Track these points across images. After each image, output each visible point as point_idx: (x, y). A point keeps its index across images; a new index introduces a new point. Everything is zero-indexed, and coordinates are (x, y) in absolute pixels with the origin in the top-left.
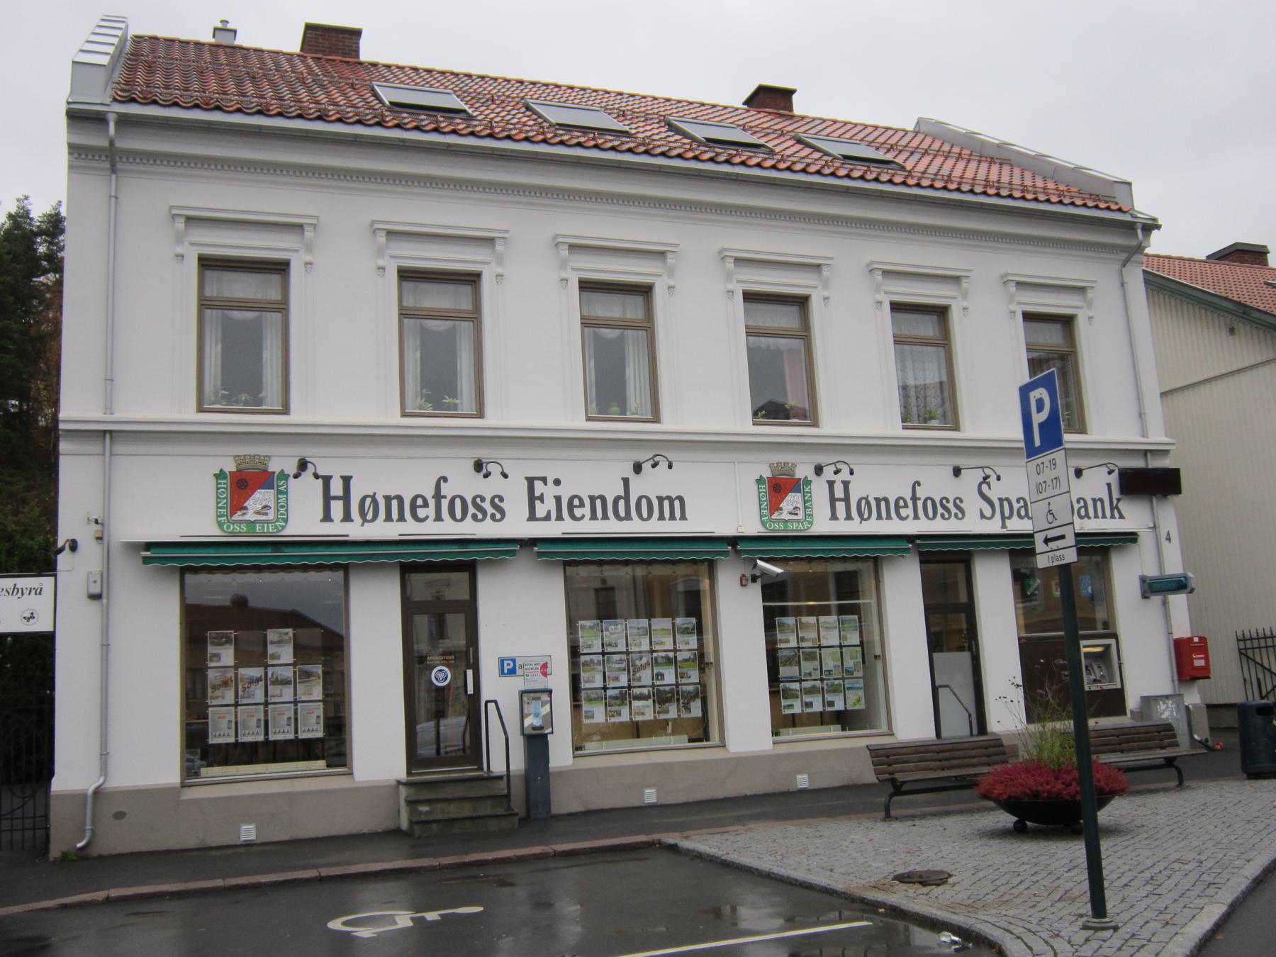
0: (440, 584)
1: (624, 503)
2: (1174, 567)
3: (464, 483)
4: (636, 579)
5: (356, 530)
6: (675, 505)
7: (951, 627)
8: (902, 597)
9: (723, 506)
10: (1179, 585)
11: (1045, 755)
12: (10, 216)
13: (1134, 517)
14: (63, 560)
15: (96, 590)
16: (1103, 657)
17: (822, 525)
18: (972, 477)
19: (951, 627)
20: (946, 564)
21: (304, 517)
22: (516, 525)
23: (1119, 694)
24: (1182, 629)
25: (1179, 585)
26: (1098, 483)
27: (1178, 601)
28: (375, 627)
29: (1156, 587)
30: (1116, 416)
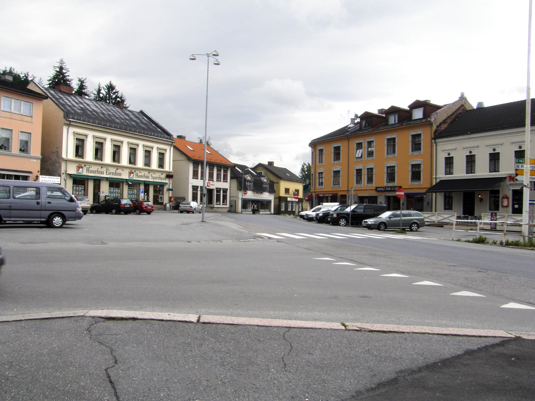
0: (97, 181)
1: (116, 174)
2: (171, 188)
3: (100, 170)
4: (115, 184)
5: (90, 174)
6: (120, 174)
7: (147, 191)
8: (142, 187)
9: (125, 176)
10: (172, 190)
11: (145, 203)
12: (26, 77)
13: (167, 181)
14: (473, 154)
15: (23, 149)
16: (161, 198)
17: (135, 178)
18: (151, 174)
19: (147, 191)
20: (147, 185)
21: (85, 173)
22: (105, 176)
23: (163, 203)
24: (171, 196)
25: (172, 190)
26: (164, 176)
27: (171, 192)
28: (91, 186)
29: (169, 190)
30: (168, 167)
